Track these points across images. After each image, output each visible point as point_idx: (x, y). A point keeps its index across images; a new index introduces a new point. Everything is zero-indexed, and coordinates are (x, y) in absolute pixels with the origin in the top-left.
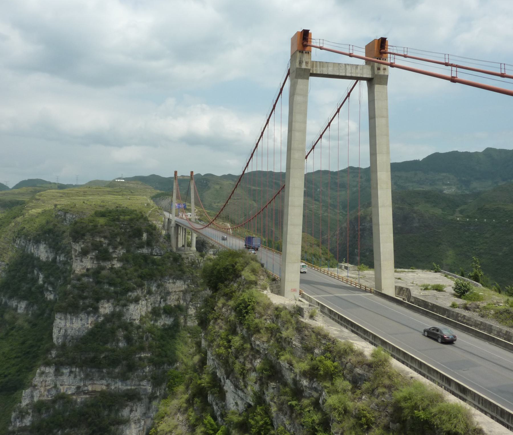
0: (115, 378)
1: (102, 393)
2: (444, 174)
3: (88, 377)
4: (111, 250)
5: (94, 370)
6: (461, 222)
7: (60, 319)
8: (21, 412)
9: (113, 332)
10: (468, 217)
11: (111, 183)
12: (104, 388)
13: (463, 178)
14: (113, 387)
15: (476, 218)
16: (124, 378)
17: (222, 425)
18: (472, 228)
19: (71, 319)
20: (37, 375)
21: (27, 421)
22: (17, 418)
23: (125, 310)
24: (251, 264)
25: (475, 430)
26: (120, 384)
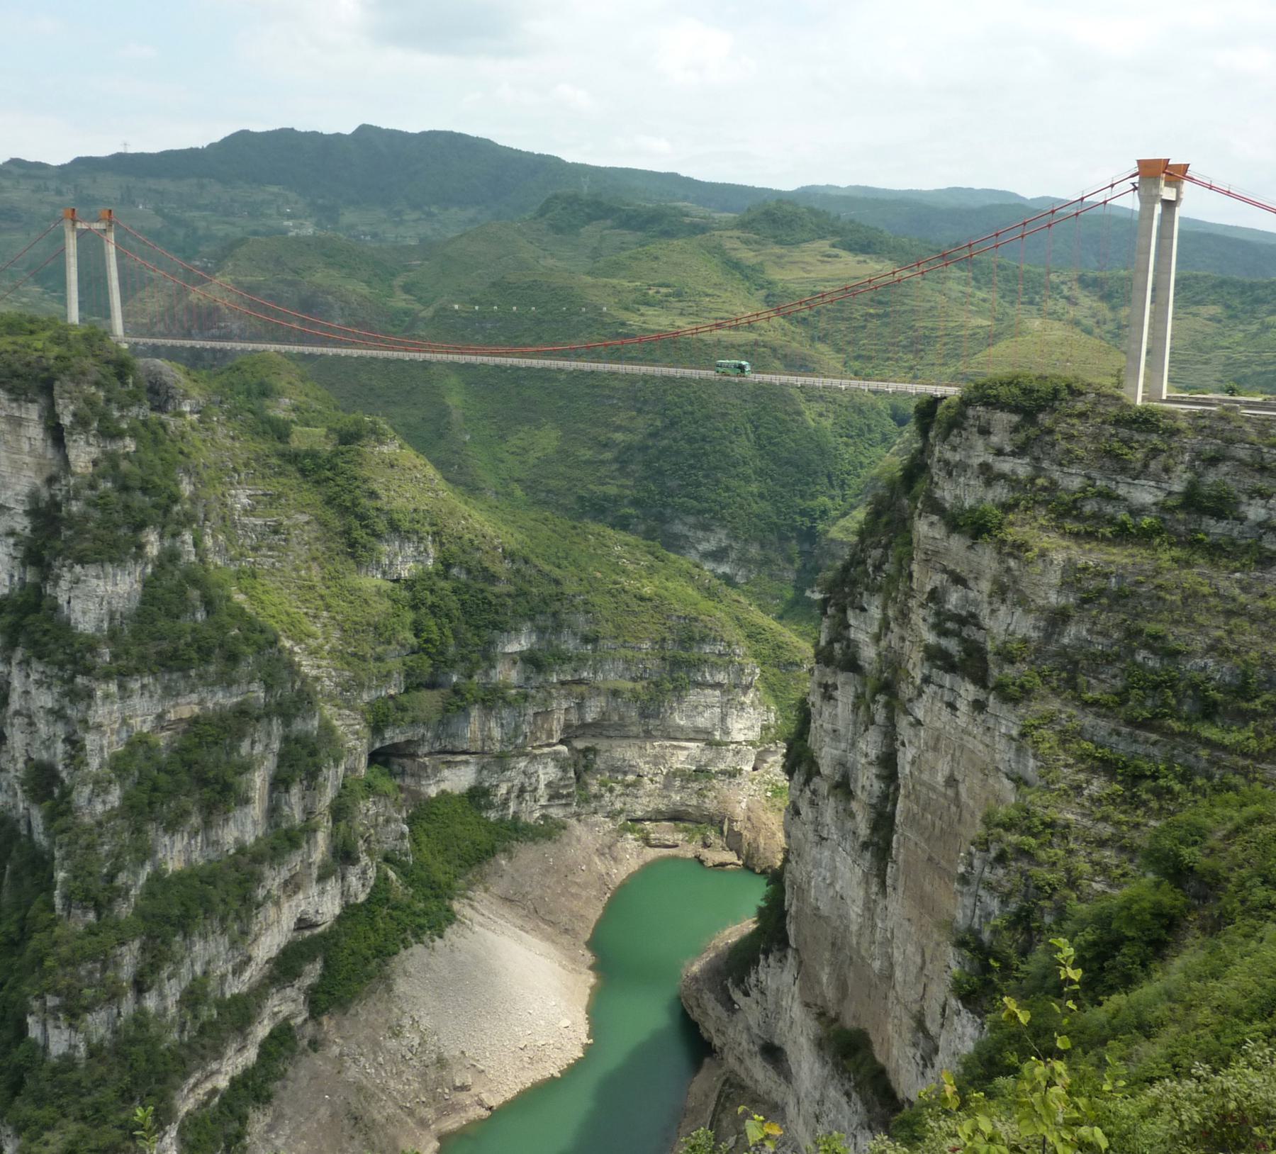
0: (213, 684)
1: (194, 721)
2: (275, 189)
3: (170, 692)
4: (116, 414)
5: (175, 676)
6: (464, 315)
7: (98, 577)
8: (97, 782)
9: (181, 593)
10: (475, 302)
11: (779, 201)
12: (197, 709)
13: (320, 201)
14: (210, 705)
15: (493, 304)
16: (226, 681)
17: (207, 839)
18: (489, 326)
19: (115, 575)
20: (99, 702)
21: (115, 797)
22: (94, 794)
23: (178, 544)
24: (45, 494)
25: (405, 875)
26: (220, 695)
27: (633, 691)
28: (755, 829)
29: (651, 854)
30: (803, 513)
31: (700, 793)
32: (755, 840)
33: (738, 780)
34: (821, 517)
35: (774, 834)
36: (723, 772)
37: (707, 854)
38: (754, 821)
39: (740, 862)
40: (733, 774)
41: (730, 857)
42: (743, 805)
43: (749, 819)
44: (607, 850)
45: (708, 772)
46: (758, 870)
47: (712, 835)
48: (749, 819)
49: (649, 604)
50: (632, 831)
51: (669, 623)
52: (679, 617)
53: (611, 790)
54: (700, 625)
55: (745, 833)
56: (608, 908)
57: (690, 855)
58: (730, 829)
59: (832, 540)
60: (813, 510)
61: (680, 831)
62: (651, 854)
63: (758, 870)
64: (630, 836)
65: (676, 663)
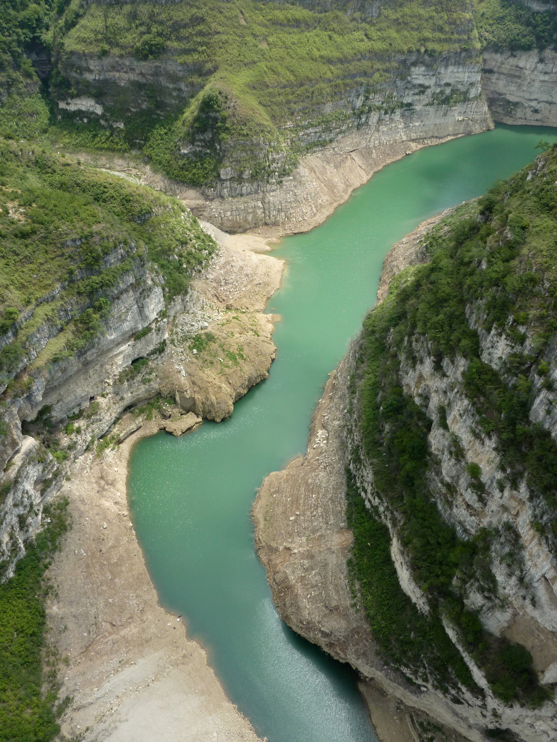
27: (69, 346)
28: (203, 389)
29: (126, 447)
30: (23, 25)
31: (144, 381)
32: (207, 399)
33: (168, 350)
34: (37, 25)
35: (220, 388)
36: (153, 352)
37: (171, 425)
38: (199, 382)
39: (200, 419)
40: (161, 349)
41: (191, 420)
42: (183, 373)
43: (194, 383)
44: (102, 482)
45: (142, 358)
46: (218, 420)
47: (168, 408)
48: (194, 383)
49: (35, 237)
50: (106, 446)
51: (67, 251)
52: (74, 241)
53: (78, 431)
54: (97, 239)
55: (197, 396)
56: (142, 539)
57: (155, 430)
58: (183, 398)
59: (72, 53)
60: (29, 19)
61: (139, 415)
62: (126, 447)
63: (218, 420)
64: (107, 451)
65: (92, 293)
